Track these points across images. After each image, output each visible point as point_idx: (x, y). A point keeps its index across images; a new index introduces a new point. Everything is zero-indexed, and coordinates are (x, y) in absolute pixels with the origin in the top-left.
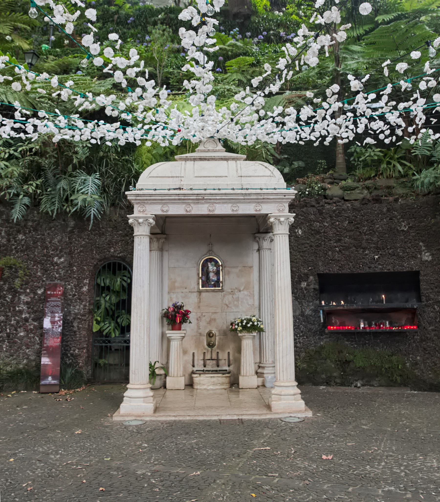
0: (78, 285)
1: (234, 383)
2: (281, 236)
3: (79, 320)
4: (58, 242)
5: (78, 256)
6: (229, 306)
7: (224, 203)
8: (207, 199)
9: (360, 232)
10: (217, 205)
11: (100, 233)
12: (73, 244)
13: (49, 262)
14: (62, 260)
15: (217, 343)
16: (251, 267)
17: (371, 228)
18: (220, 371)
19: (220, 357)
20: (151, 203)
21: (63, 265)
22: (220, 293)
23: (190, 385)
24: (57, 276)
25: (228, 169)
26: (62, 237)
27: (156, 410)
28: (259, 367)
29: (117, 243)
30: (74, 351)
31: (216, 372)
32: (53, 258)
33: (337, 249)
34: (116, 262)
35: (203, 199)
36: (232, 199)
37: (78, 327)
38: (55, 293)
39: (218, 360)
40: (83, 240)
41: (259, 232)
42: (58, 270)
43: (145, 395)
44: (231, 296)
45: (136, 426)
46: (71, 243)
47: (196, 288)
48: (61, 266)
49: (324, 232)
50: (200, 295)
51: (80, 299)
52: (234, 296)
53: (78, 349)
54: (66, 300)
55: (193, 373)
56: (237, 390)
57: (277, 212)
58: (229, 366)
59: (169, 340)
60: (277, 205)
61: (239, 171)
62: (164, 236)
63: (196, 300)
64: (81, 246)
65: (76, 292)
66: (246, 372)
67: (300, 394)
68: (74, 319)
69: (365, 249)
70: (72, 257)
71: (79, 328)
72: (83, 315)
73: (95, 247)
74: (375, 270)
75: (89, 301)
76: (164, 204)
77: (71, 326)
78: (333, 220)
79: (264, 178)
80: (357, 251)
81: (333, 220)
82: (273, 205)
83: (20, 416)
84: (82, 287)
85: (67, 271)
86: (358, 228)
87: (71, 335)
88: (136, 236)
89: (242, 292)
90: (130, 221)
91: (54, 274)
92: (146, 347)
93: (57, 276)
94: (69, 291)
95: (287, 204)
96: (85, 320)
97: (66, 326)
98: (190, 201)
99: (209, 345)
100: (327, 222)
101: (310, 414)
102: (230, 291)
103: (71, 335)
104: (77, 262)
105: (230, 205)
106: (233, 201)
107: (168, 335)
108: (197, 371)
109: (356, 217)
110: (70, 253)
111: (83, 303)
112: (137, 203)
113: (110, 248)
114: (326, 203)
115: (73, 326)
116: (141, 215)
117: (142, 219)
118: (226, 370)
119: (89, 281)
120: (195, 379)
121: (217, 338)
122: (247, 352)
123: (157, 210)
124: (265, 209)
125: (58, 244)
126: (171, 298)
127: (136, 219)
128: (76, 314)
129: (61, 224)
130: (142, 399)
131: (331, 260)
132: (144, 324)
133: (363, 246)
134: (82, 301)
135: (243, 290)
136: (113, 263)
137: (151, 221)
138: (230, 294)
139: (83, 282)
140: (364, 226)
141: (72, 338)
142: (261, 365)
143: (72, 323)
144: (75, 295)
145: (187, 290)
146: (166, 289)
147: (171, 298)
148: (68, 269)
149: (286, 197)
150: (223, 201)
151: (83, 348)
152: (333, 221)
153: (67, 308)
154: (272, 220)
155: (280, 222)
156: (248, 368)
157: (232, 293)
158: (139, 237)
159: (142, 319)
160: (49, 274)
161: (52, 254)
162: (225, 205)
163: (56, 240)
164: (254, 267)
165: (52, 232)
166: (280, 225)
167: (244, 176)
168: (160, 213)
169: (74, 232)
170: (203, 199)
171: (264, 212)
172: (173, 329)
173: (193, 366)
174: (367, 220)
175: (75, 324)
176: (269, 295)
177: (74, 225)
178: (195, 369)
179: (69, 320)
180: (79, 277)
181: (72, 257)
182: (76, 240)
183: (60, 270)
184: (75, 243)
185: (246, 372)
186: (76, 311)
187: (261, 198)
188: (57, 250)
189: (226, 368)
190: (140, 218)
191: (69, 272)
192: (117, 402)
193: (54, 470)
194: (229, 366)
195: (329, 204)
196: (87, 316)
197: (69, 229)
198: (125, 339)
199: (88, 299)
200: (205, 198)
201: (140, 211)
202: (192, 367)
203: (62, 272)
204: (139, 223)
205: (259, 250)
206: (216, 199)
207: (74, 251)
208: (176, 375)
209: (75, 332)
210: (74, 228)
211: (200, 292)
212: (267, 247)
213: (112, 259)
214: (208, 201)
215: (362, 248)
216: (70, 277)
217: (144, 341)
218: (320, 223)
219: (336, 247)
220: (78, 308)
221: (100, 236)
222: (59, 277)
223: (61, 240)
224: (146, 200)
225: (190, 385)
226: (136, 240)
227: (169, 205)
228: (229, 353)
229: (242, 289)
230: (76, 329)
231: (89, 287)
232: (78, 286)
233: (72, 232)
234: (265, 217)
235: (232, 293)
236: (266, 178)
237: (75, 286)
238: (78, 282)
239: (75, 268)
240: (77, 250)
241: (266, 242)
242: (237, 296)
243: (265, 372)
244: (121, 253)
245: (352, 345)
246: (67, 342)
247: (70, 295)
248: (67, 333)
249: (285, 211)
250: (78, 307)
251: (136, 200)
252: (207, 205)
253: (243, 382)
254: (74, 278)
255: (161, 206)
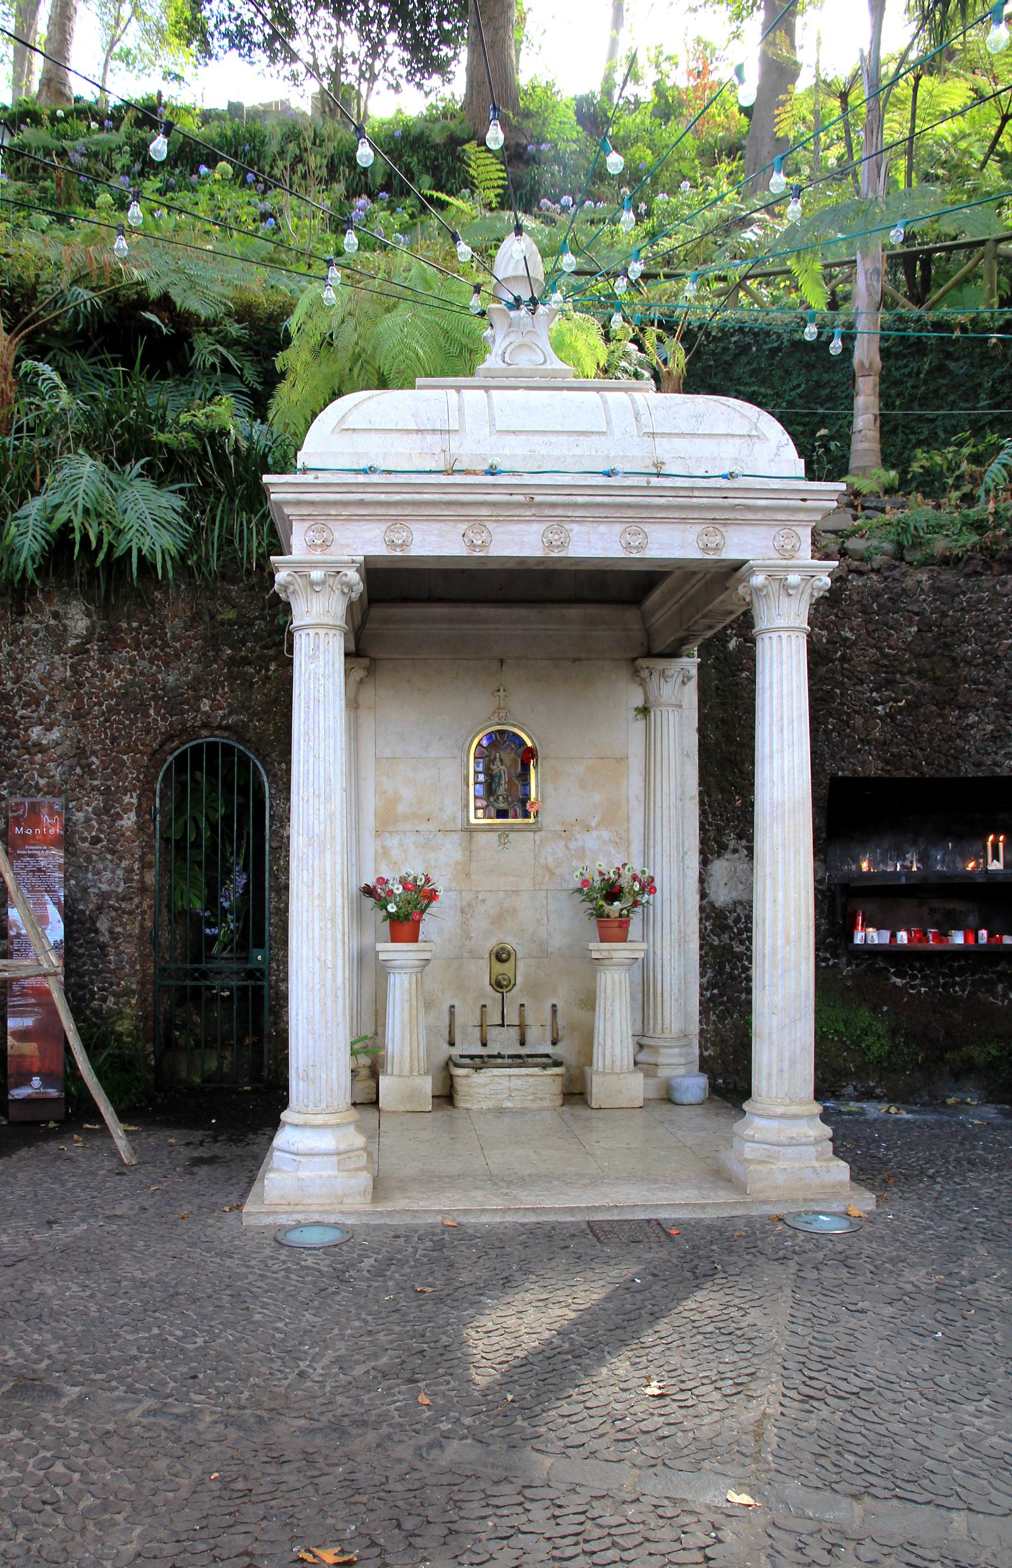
0: (106, 810)
1: (575, 1093)
2: (784, 635)
3: (113, 914)
4: (42, 681)
5: (102, 724)
6: (557, 871)
7: (597, 520)
8: (541, 505)
9: (954, 659)
10: (576, 528)
11: (167, 655)
12: (87, 688)
13: (17, 742)
14: (55, 734)
15: (519, 979)
16: (622, 759)
17: (988, 647)
18: (529, 1056)
19: (529, 1020)
20: (350, 518)
21: (59, 750)
22: (531, 834)
23: (447, 1096)
24: (42, 782)
25: (915, 90)
26: (52, 664)
27: (380, 1187)
28: (641, 1047)
29: (216, 685)
30: (104, 999)
31: (519, 1061)
32: (26, 730)
33: (879, 708)
34: (216, 743)
35: (531, 504)
36: (629, 506)
37: (111, 932)
38: (38, 831)
39: (522, 1027)
40: (117, 676)
41: (650, 654)
42: (42, 765)
43: (343, 1146)
44: (561, 843)
45: (326, 1249)
46: (80, 685)
47: (459, 821)
48: (54, 753)
49: (843, 659)
50: (470, 841)
51: (113, 852)
52: (572, 845)
53: (115, 994)
54: (73, 854)
55: (450, 1062)
56: (589, 1112)
57: (777, 555)
58: (554, 1043)
59: (382, 971)
60: (773, 531)
61: (644, 419)
62: (365, 662)
63: (458, 855)
64: (112, 695)
65: (100, 830)
66: (613, 1063)
67: (831, 1140)
68: (100, 908)
69: (965, 709)
70: (83, 726)
71: (114, 936)
72: (123, 898)
73: (156, 698)
74: (993, 772)
75: (142, 859)
76: (396, 520)
77: (90, 931)
78: (871, 621)
79: (731, 440)
80: (941, 716)
81: (871, 621)
82: (761, 531)
83: (110, 882)
84: (118, 817)
85: (72, 768)
86: (947, 646)
87: (91, 957)
88: (301, 628)
89: (595, 833)
90: (281, 577)
91: (33, 779)
92: (340, 993)
93: (42, 782)
94: (79, 828)
95: (809, 531)
96: (131, 913)
97: (77, 931)
98: (484, 511)
99: (498, 985)
100: (851, 630)
101: (864, 1202)
102: (559, 828)
103: (91, 957)
104: (102, 742)
105: (618, 528)
106: (631, 513)
107: (382, 957)
108: (462, 1056)
109: (944, 615)
110: (79, 714)
111: (124, 864)
112: (303, 518)
113: (198, 699)
114: (850, 571)
115: (97, 931)
116: (317, 556)
117: (318, 572)
118: (547, 1056)
119: (139, 798)
120: (457, 1080)
121: (520, 964)
122: (617, 1004)
123: (368, 541)
124: (737, 545)
125: (41, 688)
126: (383, 847)
127: (301, 569)
128: (104, 896)
129: (47, 627)
130: (335, 1159)
131: (861, 741)
132: (333, 921)
133: (961, 700)
134: (121, 858)
135: (596, 828)
136: (208, 743)
137: (353, 576)
138: (560, 837)
139: (119, 801)
140: (967, 641)
141: (96, 965)
142: (645, 1041)
143: (94, 923)
144: (99, 840)
145: (430, 826)
146: (369, 822)
147: (383, 847)
148: (74, 761)
149: (809, 503)
150: (598, 512)
151: (128, 992)
152: (871, 627)
153: (76, 879)
154: (758, 580)
155: (786, 588)
156: (617, 1051)
157: (566, 833)
158: (312, 632)
159: (329, 903)
160: (20, 777)
161: (22, 717)
162: (603, 528)
163: (34, 675)
164: (630, 760)
165: (21, 651)
166: (784, 600)
167: (663, 435)
168: (379, 550)
169: (87, 651)
170: (531, 504)
171: (731, 554)
172: (394, 940)
173: (452, 1044)
174: (978, 624)
175: (103, 924)
176: (674, 841)
177: (87, 629)
178: (455, 1052)
179: (83, 912)
180: (108, 788)
181: (83, 726)
182: (94, 675)
183: (51, 765)
184: (93, 686)
185: (613, 1063)
186: (105, 887)
187: (726, 501)
188: (38, 705)
189: (548, 1049)
190: (314, 565)
191: (78, 770)
192: (251, 1165)
193: (59, 1468)
194: (554, 1043)
195: (860, 573)
196: (136, 900)
197: (72, 642)
198: (249, 966)
199: (138, 853)
200: (538, 499)
201: (312, 546)
202: (446, 1046)
203: (57, 772)
204: (312, 584)
205: (644, 711)
206: (576, 505)
207: (91, 708)
208: (406, 1072)
209: (103, 947)
210: (88, 639)
211: (470, 830)
212: (673, 701)
213: (204, 733)
214: (546, 512)
215: (959, 708)
216: (81, 786)
217: (334, 975)
218: (830, 631)
219: (877, 703)
220: (109, 879)
221: (167, 665)
222: (48, 785)
223: (50, 676)
224: (335, 503)
225: (447, 1096)
226: (302, 646)
227: (414, 526)
228: (554, 1006)
229: (593, 824)
230: (105, 938)
231: (138, 815)
232: (108, 813)
233: (81, 650)
234: (735, 569)
235: (566, 833)
236: (738, 441)
237: (97, 812)
238: (106, 802)
239: (94, 759)
240: (101, 704)
241: (671, 682)
242: (580, 843)
243: (661, 1060)
244: (230, 714)
245: (913, 987)
246: (82, 976)
247: (84, 840)
248: (81, 951)
249: (801, 554)
250: (108, 875)
251: (298, 503)
252: (538, 528)
253: (599, 1089)
254: (94, 788)
255: (383, 526)
